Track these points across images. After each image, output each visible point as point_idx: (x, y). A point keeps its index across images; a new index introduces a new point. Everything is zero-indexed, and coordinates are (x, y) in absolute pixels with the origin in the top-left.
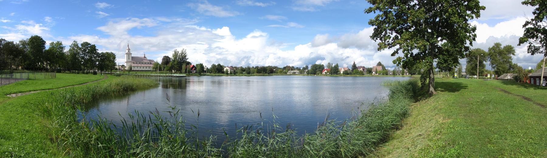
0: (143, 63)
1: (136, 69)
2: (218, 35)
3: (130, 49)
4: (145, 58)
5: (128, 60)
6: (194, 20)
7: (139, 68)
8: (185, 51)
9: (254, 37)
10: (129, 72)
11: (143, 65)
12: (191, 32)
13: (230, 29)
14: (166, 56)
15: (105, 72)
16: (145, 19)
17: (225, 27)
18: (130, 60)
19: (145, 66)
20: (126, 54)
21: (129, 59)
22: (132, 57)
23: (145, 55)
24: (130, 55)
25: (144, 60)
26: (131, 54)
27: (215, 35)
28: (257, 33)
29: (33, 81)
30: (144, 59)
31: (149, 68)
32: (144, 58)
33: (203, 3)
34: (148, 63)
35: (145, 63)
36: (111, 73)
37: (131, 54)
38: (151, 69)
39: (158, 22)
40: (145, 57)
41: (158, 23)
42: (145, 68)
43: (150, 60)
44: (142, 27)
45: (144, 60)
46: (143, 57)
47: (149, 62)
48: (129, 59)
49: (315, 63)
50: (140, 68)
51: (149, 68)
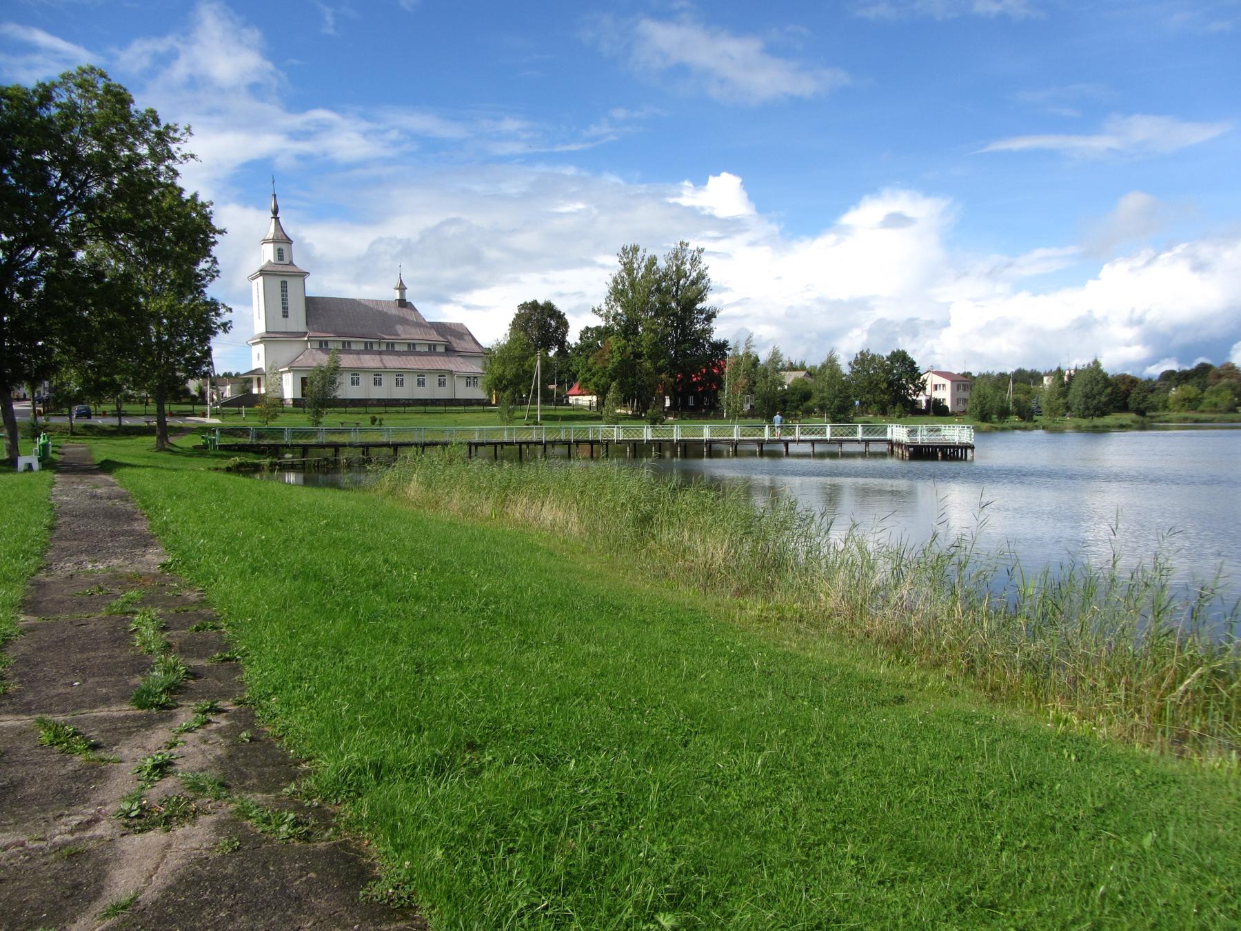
0: (391, 349)
1: (365, 390)
2: (711, 217)
3: (289, 242)
4: (404, 312)
5: (282, 325)
6: (594, 130)
7: (366, 380)
8: (694, 261)
9: (896, 220)
10: (318, 414)
11: (392, 362)
12: (571, 198)
13: (745, 185)
14: (534, 305)
15: (85, 422)
16: (321, 114)
17: (717, 174)
18: (297, 321)
19: (410, 372)
20: (263, 272)
21: (285, 314)
22: (313, 305)
23: (402, 288)
24: (292, 284)
25: (399, 329)
26: (303, 275)
27: (693, 212)
28: (902, 202)
29: (457, 415)
30: (404, 321)
31: (442, 383)
32: (395, 311)
33: (665, 15)
34: (432, 350)
35: (412, 349)
36: (162, 422)
37: (303, 275)
38: (479, 393)
39: (394, 135)
40: (403, 303)
41: (395, 144)
42: (410, 381)
43: (441, 328)
44: (301, 157)
45: (399, 329)
46: (387, 303)
47: (434, 336)
48: (285, 314)
49: (1228, 354)
50: (377, 383)
51: (442, 383)
